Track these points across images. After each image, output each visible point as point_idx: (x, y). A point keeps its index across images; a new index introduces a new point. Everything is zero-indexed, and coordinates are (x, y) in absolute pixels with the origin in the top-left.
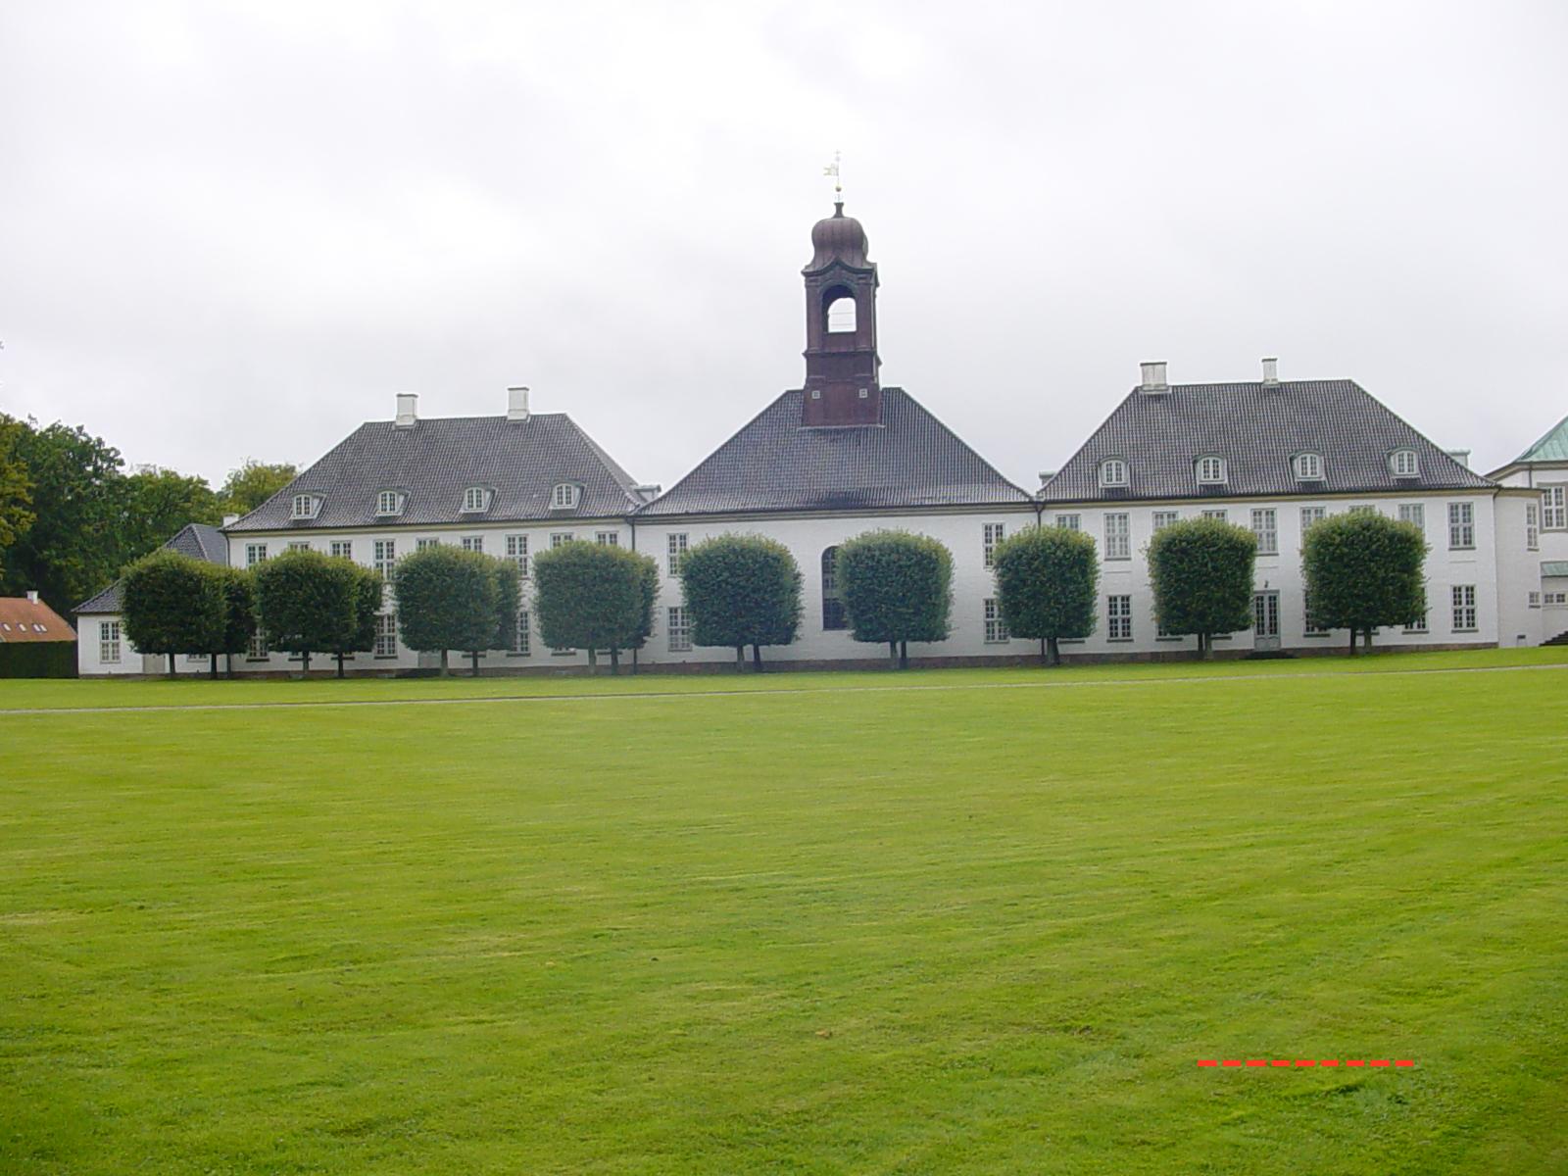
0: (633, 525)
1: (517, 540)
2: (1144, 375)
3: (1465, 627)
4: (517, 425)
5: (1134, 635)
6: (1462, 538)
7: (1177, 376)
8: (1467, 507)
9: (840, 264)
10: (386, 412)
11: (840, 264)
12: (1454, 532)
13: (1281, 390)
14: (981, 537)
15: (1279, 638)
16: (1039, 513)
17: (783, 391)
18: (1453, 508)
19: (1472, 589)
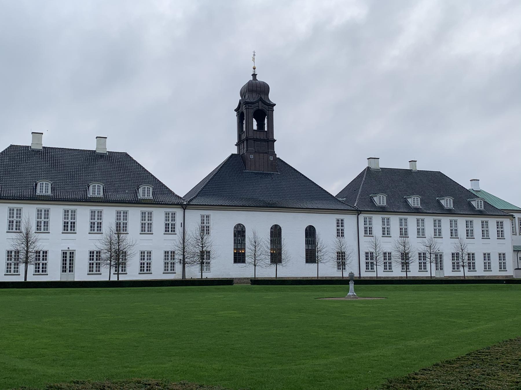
0: (184, 210)
1: (43, 211)
2: (369, 163)
3: (145, 271)
4: (37, 152)
5: (477, 269)
6: (146, 228)
7: (383, 164)
8: (150, 213)
9: (256, 106)
10: (26, 141)
11: (256, 106)
12: (167, 225)
13: (48, 153)
14: (381, 223)
15: (74, 275)
16: (184, 210)
17: (230, 154)
18: (118, 213)
19: (46, 252)
